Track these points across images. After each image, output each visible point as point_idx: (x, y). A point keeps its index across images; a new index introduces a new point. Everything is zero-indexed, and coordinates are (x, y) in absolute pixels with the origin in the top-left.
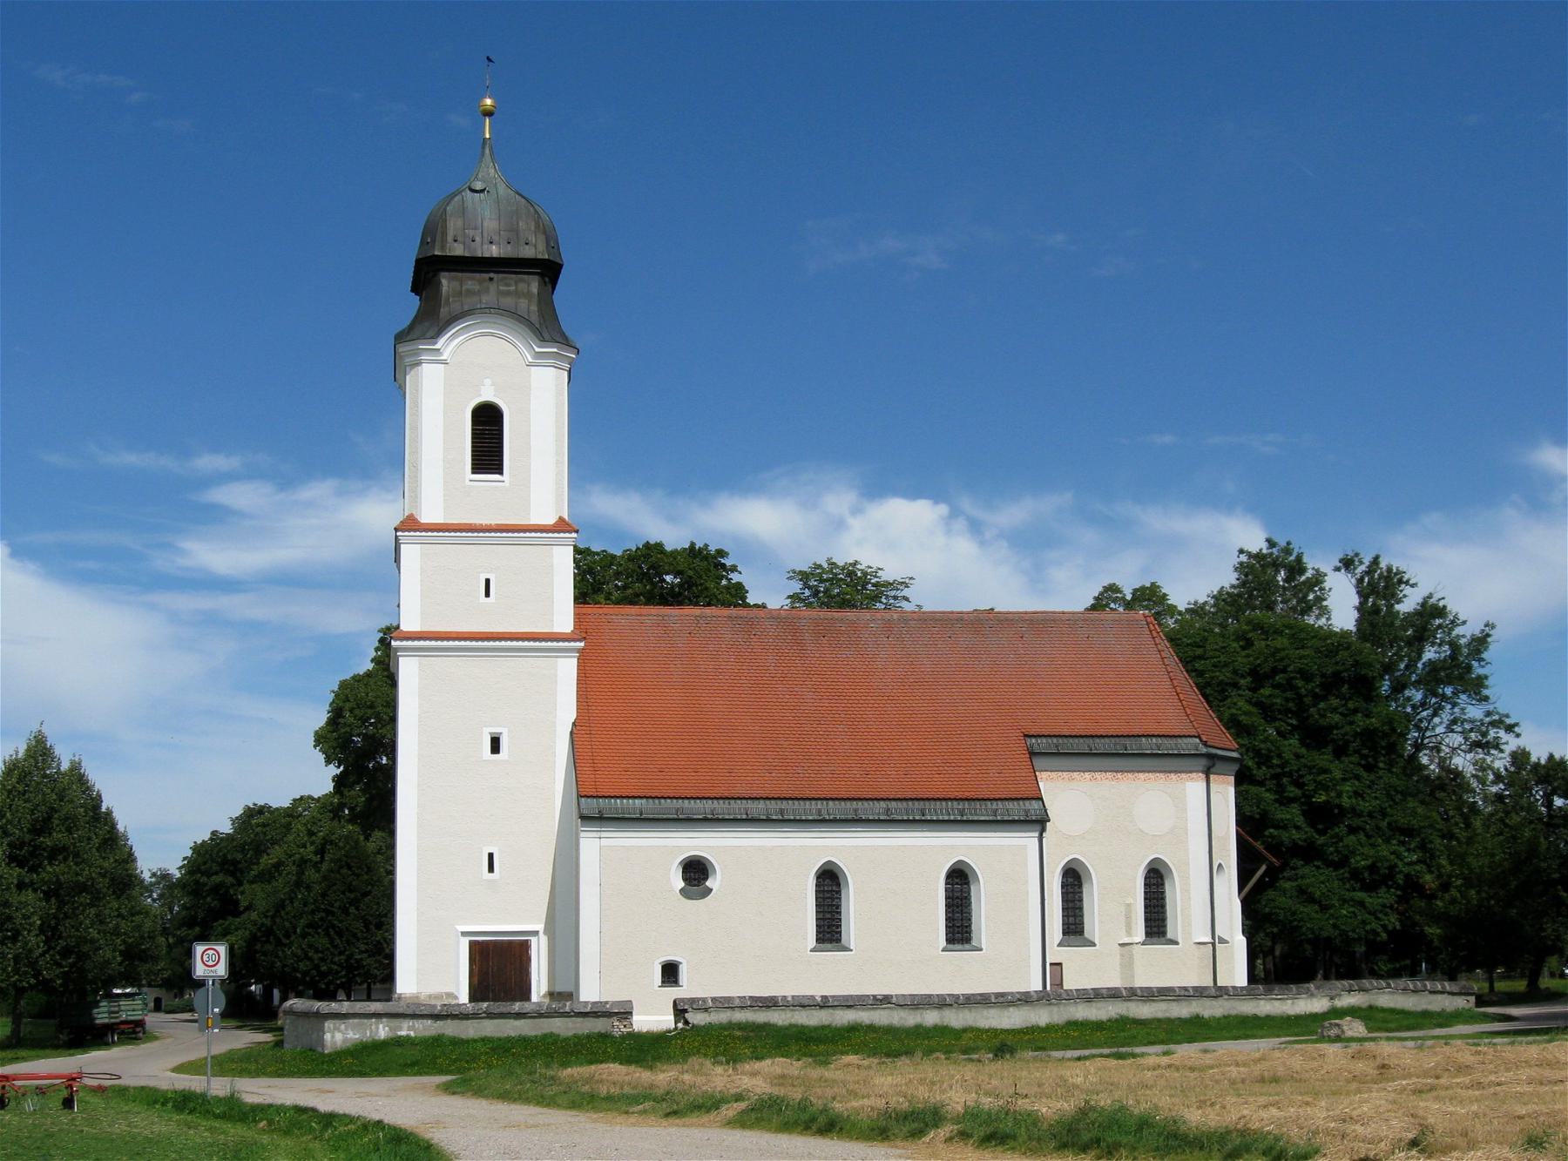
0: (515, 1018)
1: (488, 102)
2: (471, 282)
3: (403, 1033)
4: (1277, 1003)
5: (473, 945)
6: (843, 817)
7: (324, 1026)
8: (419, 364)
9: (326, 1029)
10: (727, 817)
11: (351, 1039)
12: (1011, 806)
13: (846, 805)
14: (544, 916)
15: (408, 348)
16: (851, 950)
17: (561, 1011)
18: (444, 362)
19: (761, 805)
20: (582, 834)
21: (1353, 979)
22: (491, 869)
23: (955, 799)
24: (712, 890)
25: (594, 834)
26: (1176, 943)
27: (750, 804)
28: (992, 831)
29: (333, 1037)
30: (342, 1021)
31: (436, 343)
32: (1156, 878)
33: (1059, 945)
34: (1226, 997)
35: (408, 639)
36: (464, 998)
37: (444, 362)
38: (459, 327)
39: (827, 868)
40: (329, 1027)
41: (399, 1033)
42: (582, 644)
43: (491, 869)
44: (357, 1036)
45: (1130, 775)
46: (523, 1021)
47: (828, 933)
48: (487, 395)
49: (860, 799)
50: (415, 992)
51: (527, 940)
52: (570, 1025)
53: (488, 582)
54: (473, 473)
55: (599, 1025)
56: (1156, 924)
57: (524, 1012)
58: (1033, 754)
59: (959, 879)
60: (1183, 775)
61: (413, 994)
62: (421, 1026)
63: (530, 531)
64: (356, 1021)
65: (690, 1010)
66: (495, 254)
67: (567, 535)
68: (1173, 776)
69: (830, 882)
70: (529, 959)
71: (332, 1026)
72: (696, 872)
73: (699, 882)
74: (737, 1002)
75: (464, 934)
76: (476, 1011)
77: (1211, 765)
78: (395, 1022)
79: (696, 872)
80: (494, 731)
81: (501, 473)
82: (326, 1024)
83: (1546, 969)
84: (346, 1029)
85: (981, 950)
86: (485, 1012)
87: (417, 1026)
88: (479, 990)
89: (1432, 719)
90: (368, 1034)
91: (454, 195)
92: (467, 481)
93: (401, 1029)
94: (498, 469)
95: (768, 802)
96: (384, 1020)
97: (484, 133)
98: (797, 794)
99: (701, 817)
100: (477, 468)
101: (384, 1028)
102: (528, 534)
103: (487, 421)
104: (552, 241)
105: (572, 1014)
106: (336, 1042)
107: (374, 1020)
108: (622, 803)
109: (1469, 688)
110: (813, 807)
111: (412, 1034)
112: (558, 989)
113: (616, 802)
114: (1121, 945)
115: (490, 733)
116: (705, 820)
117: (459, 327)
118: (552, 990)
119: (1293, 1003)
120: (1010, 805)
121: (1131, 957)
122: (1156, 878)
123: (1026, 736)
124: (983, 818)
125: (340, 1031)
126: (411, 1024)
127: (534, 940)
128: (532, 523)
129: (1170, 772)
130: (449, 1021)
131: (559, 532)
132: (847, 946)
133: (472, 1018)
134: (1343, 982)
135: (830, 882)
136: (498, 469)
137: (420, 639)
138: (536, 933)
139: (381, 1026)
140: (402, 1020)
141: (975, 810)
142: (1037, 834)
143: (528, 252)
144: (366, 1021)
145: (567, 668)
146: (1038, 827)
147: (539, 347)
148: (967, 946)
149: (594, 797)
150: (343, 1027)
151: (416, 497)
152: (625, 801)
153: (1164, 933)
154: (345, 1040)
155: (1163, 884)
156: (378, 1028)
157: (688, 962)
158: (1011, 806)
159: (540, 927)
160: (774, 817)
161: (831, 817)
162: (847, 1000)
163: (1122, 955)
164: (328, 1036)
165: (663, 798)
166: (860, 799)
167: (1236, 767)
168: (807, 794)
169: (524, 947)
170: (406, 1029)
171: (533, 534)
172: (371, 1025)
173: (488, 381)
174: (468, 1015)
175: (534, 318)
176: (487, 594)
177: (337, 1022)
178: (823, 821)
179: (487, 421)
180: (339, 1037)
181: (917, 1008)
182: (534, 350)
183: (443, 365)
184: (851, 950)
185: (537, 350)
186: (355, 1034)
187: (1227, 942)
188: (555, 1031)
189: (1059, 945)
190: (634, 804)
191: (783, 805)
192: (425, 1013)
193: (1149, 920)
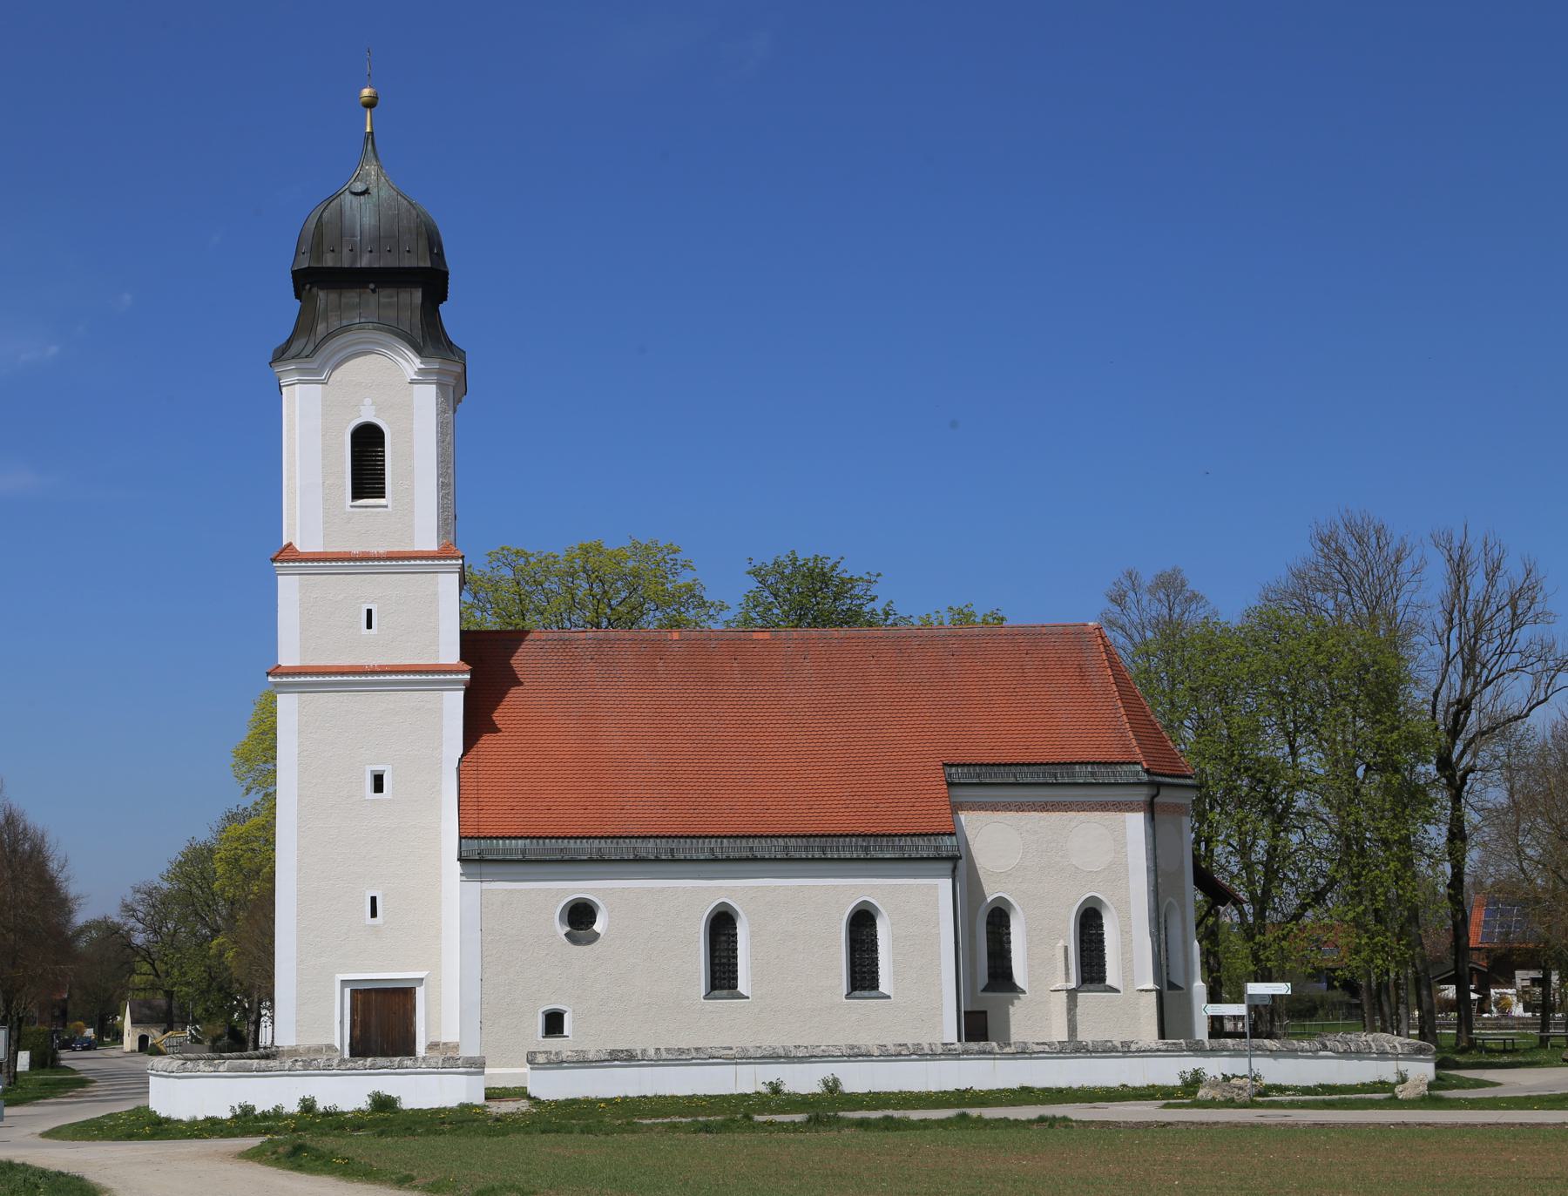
6: (737, 855)
10: (508, 857)
12: (921, 843)
13: (741, 842)
19: (651, 844)
22: (374, 914)
23: (859, 836)
27: (639, 844)
32: (1090, 921)
33: (984, 990)
35: (287, 674)
39: (722, 909)
43: (374, 914)
47: (864, 972)
49: (755, 837)
53: (369, 612)
56: (1091, 967)
58: (950, 785)
59: (862, 924)
61: (292, 1047)
63: (415, 558)
67: (454, 562)
69: (722, 925)
72: (580, 916)
73: (587, 926)
77: (1155, 792)
79: (580, 916)
81: (381, 494)
91: (331, 199)
94: (380, 493)
95: (658, 841)
97: (366, 129)
99: (586, 858)
100: (357, 494)
103: (368, 441)
104: (433, 243)
108: (504, 844)
110: (706, 845)
113: (498, 844)
115: (372, 771)
116: (591, 860)
120: (920, 842)
122: (1090, 921)
131: (445, 558)
135: (722, 925)
136: (380, 493)
137: (299, 674)
141: (881, 846)
143: (409, 262)
145: (453, 703)
148: (873, 993)
149: (476, 838)
152: (507, 841)
153: (1103, 979)
158: (921, 843)
160: (663, 857)
165: (546, 837)
166: (755, 837)
167: (1142, 794)
168: (776, 831)
173: (368, 401)
175: (418, 334)
176: (369, 626)
179: (368, 441)
183: (320, 386)
187: (1179, 988)
189: (984, 990)
190: (517, 844)
191: (674, 844)
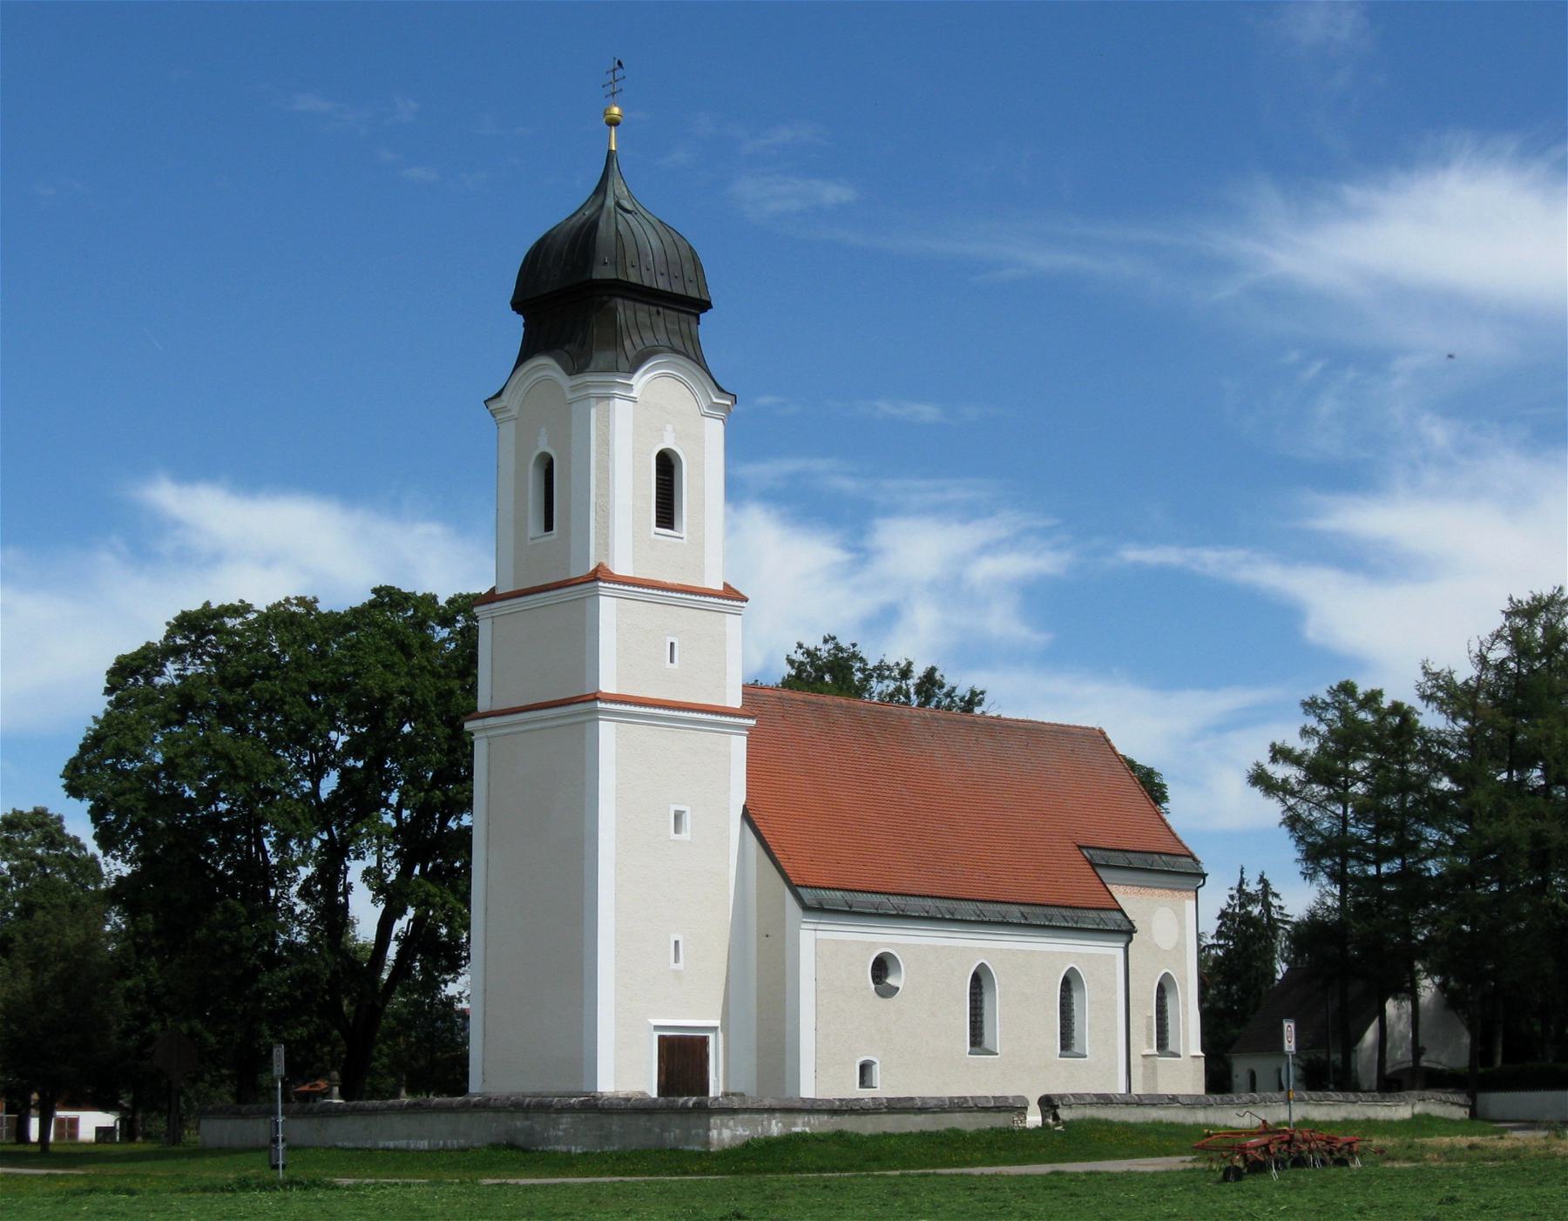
0: (915, 1114)
1: (616, 110)
2: (643, 313)
3: (798, 1129)
4: (1386, 1109)
5: (662, 1039)
7: (709, 1123)
8: (610, 397)
9: (712, 1125)
11: (741, 1135)
14: (720, 1011)
15: (594, 379)
16: (997, 1054)
17: (965, 1105)
18: (633, 400)
20: (803, 926)
21: (1320, 1090)
24: (898, 989)
25: (812, 926)
26: (1179, 1056)
28: (1073, 938)
29: (720, 1134)
30: (732, 1117)
31: (631, 378)
34: (1360, 1103)
36: (654, 1094)
37: (633, 400)
38: (651, 364)
40: (715, 1124)
41: (793, 1129)
42: (752, 722)
44: (747, 1133)
45: (1149, 891)
46: (923, 1116)
48: (668, 443)
50: (613, 1090)
51: (705, 1037)
52: (971, 1120)
54: (657, 526)
55: (1000, 1121)
57: (928, 1106)
60: (1184, 894)
62: (817, 1122)
64: (746, 1116)
65: (1061, 1106)
66: (661, 287)
68: (1176, 893)
70: (707, 1056)
71: (719, 1122)
74: (1088, 1100)
75: (657, 1028)
76: (877, 1107)
78: (789, 1118)
79: (882, 967)
80: (678, 809)
82: (712, 1121)
83: (686, 1098)
84: (735, 1126)
85: (1085, 1056)
86: (886, 1107)
87: (812, 1122)
88: (666, 1087)
89: (1426, 859)
90: (760, 1130)
92: (653, 533)
93: (795, 1124)
96: (777, 1115)
98: (900, 890)
101: (777, 1125)
102: (708, 599)
105: (975, 1108)
106: (723, 1139)
107: (766, 1116)
109: (256, 779)
111: (807, 1130)
112: (731, 1090)
114: (1144, 1056)
117: (651, 364)
118: (726, 1091)
119: (1396, 1110)
121: (1154, 1068)
123: (1080, 847)
124: (1090, 927)
125: (727, 1127)
126: (806, 1119)
127: (711, 1036)
128: (706, 587)
129: (1175, 890)
130: (846, 1116)
132: (993, 1050)
133: (873, 1113)
134: (1216, 1096)
138: (714, 1029)
139: (774, 1122)
140: (796, 1115)
142: (1123, 945)
144: (756, 1116)
145: (738, 746)
146: (1125, 938)
147: (717, 397)
150: (731, 1123)
151: (607, 545)
154: (734, 1138)
155: (981, 994)
156: (770, 1124)
157: (881, 1062)
159: (717, 1023)
161: (987, 919)
162: (1153, 1099)
163: (1145, 1066)
164: (714, 1134)
169: (704, 1042)
170: (801, 1126)
171: (712, 600)
172: (763, 1121)
174: (868, 1110)
177: (725, 1118)
178: (982, 923)
180: (726, 1134)
181: (1194, 1108)
182: (711, 399)
183: (631, 403)
184: (997, 1054)
185: (715, 400)
186: (744, 1131)
188: (957, 1126)
192: (824, 1107)
193: (972, 1035)
